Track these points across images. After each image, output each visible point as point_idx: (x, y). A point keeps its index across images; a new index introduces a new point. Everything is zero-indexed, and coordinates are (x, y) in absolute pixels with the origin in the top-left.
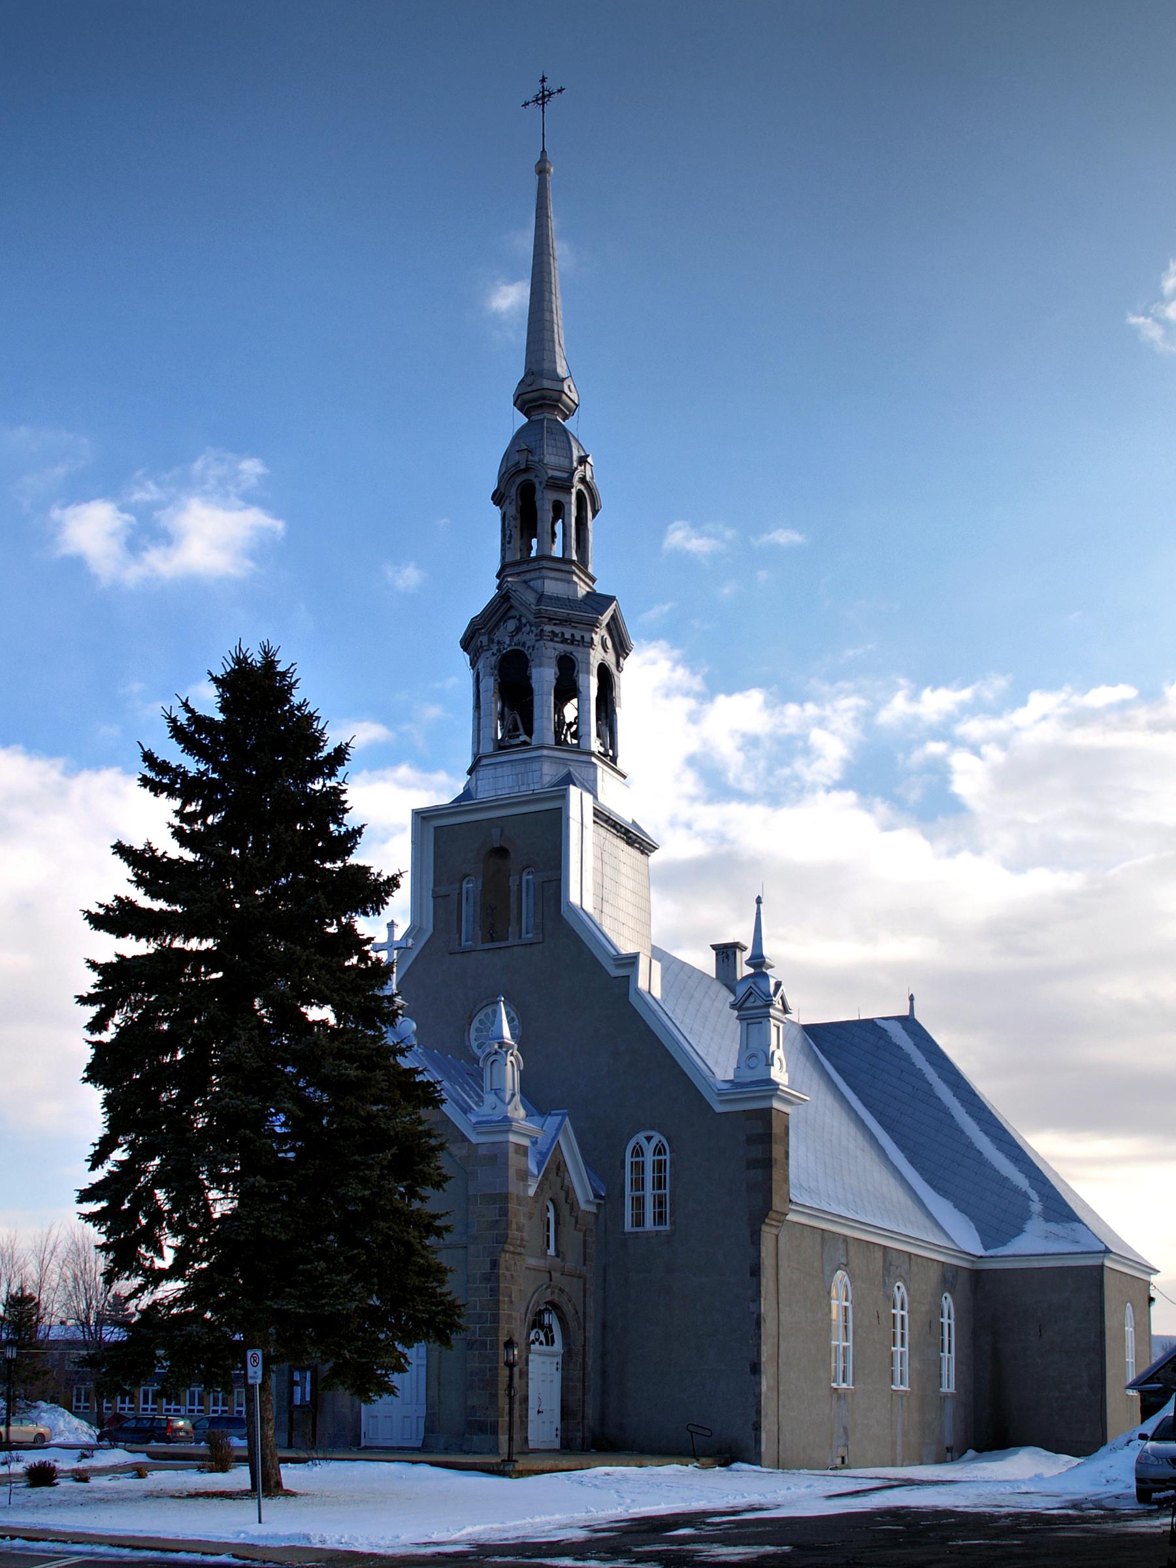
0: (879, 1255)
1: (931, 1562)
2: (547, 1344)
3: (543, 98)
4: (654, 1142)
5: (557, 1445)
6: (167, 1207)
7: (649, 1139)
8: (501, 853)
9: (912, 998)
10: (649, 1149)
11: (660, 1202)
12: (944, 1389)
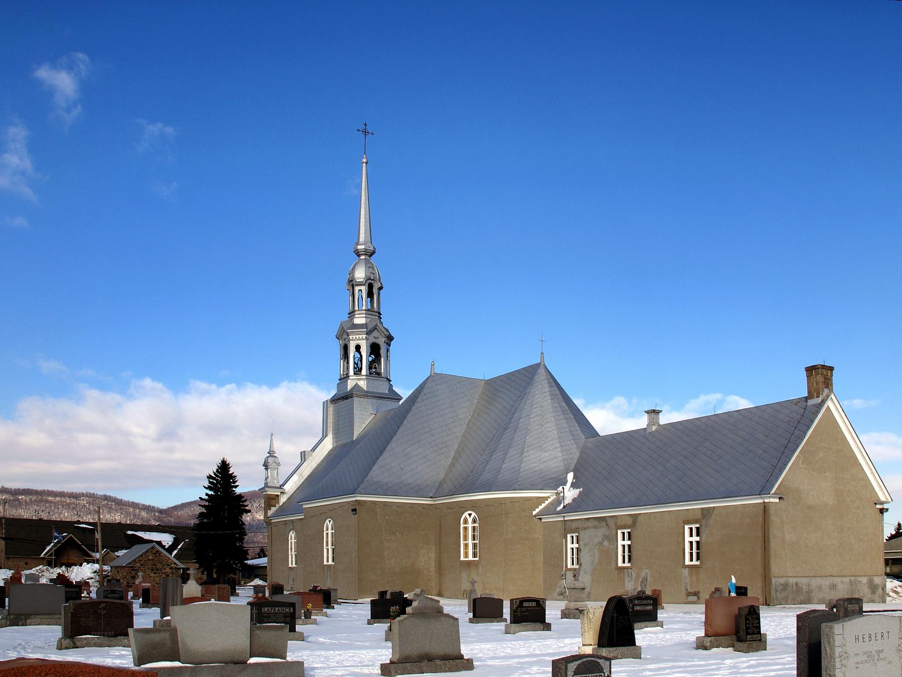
1: (513, 669)
3: (365, 132)
6: (292, 610)
7: (470, 515)
10: (470, 520)
11: (475, 545)
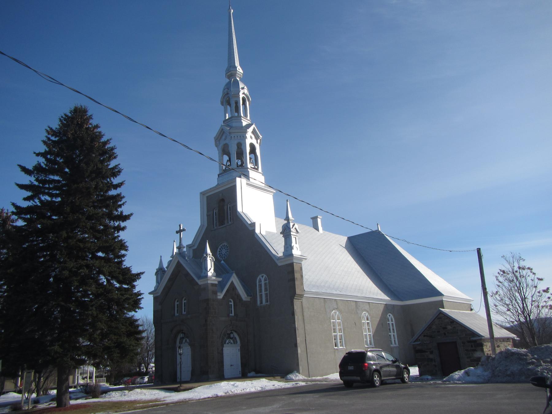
0: (354, 303)
2: (234, 343)
4: (264, 277)
5: (241, 375)
7: (262, 276)
8: (223, 200)
9: (161, 257)
10: (263, 279)
12: (393, 345)
